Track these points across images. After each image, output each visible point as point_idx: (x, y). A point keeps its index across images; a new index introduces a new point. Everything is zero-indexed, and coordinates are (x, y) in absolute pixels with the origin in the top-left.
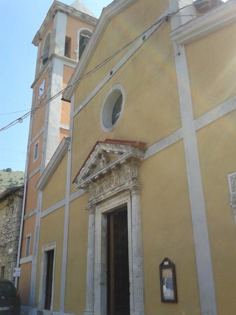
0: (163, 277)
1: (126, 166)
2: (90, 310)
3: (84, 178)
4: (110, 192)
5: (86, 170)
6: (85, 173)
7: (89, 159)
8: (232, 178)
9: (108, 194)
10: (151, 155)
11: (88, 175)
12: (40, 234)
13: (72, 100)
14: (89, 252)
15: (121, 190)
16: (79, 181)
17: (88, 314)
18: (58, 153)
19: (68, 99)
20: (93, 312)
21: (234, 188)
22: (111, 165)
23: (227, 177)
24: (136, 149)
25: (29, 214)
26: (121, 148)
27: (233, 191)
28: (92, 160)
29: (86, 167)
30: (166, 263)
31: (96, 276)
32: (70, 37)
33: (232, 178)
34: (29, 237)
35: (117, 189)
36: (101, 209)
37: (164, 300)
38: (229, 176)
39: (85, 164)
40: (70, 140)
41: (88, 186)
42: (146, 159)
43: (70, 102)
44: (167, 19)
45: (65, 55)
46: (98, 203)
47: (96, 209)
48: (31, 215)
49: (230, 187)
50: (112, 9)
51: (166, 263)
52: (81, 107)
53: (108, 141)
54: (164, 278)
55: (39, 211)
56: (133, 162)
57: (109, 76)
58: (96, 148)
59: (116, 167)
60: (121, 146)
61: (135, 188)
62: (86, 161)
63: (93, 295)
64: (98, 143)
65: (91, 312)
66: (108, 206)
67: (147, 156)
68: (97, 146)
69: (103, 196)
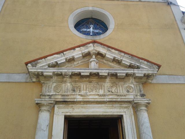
4: (97, 97)
5: (61, 59)
7: (72, 51)
9: (91, 97)
11: (56, 65)
15: (119, 100)
16: (39, 65)
29: (62, 56)
35: (111, 97)
42: (153, 84)
47: (56, 106)
61: (147, 105)
68: (91, 45)
69: (79, 97)
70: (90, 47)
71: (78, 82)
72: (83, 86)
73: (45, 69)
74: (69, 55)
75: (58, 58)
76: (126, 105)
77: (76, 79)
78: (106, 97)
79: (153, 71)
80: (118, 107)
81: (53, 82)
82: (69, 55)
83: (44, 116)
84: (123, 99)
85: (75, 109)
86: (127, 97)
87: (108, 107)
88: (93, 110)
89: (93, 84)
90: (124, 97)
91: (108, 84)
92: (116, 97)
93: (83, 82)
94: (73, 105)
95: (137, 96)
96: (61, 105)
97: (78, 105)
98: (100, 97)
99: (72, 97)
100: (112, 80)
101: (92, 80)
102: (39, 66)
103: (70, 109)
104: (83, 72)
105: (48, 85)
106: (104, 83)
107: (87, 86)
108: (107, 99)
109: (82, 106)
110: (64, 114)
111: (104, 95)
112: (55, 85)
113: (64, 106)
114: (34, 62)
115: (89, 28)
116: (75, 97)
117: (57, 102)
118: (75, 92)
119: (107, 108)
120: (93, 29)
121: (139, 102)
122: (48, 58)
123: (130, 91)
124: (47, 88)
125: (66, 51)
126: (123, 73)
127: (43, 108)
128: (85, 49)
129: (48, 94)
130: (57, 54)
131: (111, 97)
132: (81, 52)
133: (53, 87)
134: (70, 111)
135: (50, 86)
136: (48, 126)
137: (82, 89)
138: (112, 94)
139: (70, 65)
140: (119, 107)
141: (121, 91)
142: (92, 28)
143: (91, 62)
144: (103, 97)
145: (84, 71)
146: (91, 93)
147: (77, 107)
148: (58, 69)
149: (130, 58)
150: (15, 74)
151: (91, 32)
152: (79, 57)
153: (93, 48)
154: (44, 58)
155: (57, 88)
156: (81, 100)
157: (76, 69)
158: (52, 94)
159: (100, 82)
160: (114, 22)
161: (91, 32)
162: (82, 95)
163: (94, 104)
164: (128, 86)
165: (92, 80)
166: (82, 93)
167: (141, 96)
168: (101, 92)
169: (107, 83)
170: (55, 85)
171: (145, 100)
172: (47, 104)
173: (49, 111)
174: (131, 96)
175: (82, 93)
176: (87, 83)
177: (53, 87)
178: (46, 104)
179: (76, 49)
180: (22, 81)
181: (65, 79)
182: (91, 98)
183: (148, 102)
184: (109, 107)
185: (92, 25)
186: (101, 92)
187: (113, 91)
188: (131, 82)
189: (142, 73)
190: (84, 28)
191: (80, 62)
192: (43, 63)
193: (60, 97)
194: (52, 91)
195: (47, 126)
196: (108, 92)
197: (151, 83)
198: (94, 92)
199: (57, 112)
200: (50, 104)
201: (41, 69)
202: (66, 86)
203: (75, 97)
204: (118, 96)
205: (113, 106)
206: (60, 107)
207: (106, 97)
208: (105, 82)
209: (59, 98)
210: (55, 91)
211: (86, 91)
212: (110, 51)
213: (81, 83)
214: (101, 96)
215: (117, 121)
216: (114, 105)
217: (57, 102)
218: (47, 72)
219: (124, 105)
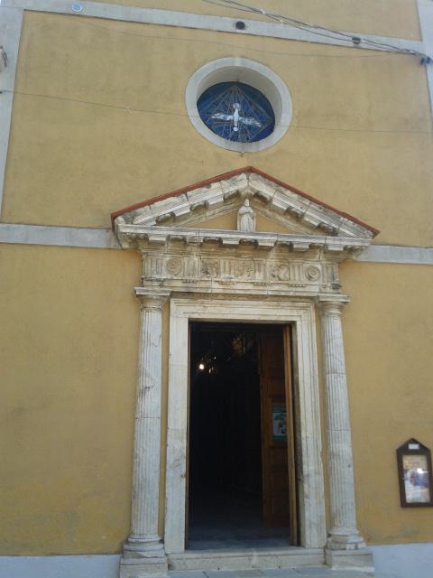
0: (404, 467)
1: (195, 250)
3: (161, 221)
4: (250, 287)
5: (180, 206)
7: (204, 189)
9: (239, 286)
11: (172, 219)
14: (151, 403)
15: (291, 294)
16: (139, 220)
20: (162, 541)
22: (297, 240)
30: (413, 447)
31: (170, 459)
35: (277, 288)
36: (192, 309)
39: (184, 191)
42: (360, 262)
46: (189, 295)
47: (173, 305)
48: (263, 148)
51: (413, 447)
54: (407, 470)
63: (162, 510)
64: (250, 170)
68: (243, 176)
75: (176, 204)
82: (198, 197)
83: (153, 319)
84: (300, 292)
86: (306, 289)
88: (241, 310)
92: (286, 288)
93: (227, 255)
95: (325, 287)
96: (182, 300)
98: (256, 288)
99: (203, 284)
102: (139, 221)
104: (227, 239)
108: (268, 291)
110: (187, 316)
112: (168, 259)
113: (187, 301)
115: (231, 112)
117: (174, 294)
122: (157, 204)
124: (154, 265)
127: (151, 305)
131: (277, 288)
135: (159, 262)
137: (222, 270)
141: (297, 278)
142: (237, 111)
144: (261, 288)
145: (228, 236)
146: (240, 279)
151: (236, 125)
161: (236, 125)
162: (222, 283)
166: (223, 277)
168: (259, 277)
171: (339, 298)
174: (314, 287)
175: (223, 277)
182: (239, 288)
186: (259, 277)
187: (282, 276)
189: (340, 246)
190: (219, 111)
193: (180, 284)
197: (355, 261)
198: (245, 278)
204: (291, 286)
205: (278, 305)
209: (179, 286)
210: (169, 272)
212: (281, 192)
214: (257, 284)
216: (282, 304)
217: (174, 294)
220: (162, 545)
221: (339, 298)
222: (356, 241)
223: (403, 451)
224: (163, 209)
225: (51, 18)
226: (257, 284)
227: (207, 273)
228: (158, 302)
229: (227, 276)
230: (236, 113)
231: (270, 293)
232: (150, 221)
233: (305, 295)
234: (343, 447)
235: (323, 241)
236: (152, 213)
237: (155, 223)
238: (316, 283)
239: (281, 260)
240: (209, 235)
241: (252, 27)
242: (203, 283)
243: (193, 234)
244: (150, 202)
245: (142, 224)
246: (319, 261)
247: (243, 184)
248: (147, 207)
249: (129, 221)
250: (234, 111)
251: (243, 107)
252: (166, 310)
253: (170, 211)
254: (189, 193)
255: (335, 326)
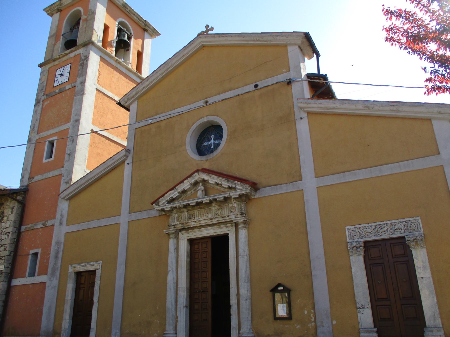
2: (172, 332)
3: (170, 202)
4: (206, 221)
5: (174, 194)
6: (172, 197)
7: (182, 184)
8: (349, 230)
9: (202, 222)
10: (263, 196)
11: (172, 200)
12: (63, 251)
13: (134, 107)
14: (171, 277)
15: (223, 221)
16: (161, 203)
17: (172, 335)
18: (110, 163)
19: (126, 105)
20: (176, 333)
21: (350, 237)
23: (345, 229)
24: (253, 188)
25: (36, 225)
26: (236, 184)
27: (349, 239)
28: (186, 185)
29: (175, 191)
30: (280, 288)
32: (109, 26)
33: (349, 230)
34: (36, 254)
35: (217, 219)
37: (276, 318)
38: (347, 228)
40: (130, 153)
41: (173, 210)
42: (256, 198)
43: (128, 110)
44: (289, 82)
45: (102, 46)
47: (180, 235)
49: (347, 236)
50: (238, 38)
51: (280, 288)
52: (150, 121)
53: (205, 171)
55: (61, 224)
56: (244, 198)
57: (202, 103)
58: (194, 175)
59: (224, 199)
60: (235, 182)
61: (245, 223)
62: (177, 185)
63: (176, 317)
64: (197, 171)
65: (173, 333)
66: (200, 233)
67: (257, 195)
68: (196, 174)
69: (193, 223)
70: (195, 176)
71: (192, 210)
72: (197, 213)
73: (165, 206)
74: (180, 188)
75: (172, 193)
76: (230, 224)
77: (190, 209)
78: (214, 220)
79: (246, 190)
80: (224, 227)
81: (175, 214)
82: (180, 188)
83: (172, 242)
84: (226, 219)
85: (194, 233)
86: (230, 217)
87: (217, 228)
88: (206, 232)
89: (204, 209)
90: (227, 218)
91: (215, 207)
92: (220, 219)
93: (196, 209)
94: (192, 231)
95: (237, 215)
96: (183, 232)
97: (195, 230)
98: (209, 221)
99: (189, 224)
100: (217, 204)
101: (201, 206)
102: (161, 204)
103: (190, 234)
104: (191, 203)
105: (172, 216)
106: (212, 208)
107: (200, 212)
108: (214, 222)
109: (198, 230)
110: (186, 238)
111: (211, 219)
112: (177, 215)
113: (185, 232)
114: (156, 202)
115: (210, 140)
116: (191, 223)
117: (181, 230)
118: (191, 219)
119: (216, 229)
120: (214, 140)
121: (237, 221)
122: (166, 195)
123: (232, 211)
124: (172, 220)
125: (177, 186)
126: (221, 197)
127: (171, 236)
128: (192, 179)
129: (172, 224)
130: (171, 190)
131: (217, 219)
132: (189, 183)
133: (176, 217)
134: (190, 236)
135: (174, 217)
136: (176, 249)
137: (196, 216)
138: (218, 216)
139: (185, 195)
140: (225, 227)
141: (225, 213)
142: (213, 138)
143: (198, 191)
144: (211, 221)
145: (191, 202)
146: (203, 218)
147: (194, 231)
148: (174, 204)
149: (227, 180)
150: (151, 210)
151: (212, 145)
152: (189, 188)
153: (198, 177)
154: (163, 196)
155: (178, 218)
156: (195, 225)
157: (185, 202)
158: (175, 224)
159: (209, 207)
160: (227, 131)
161: (212, 145)
162: (195, 222)
163: (207, 227)
164: (231, 206)
165: (201, 206)
166: (196, 220)
167: (241, 215)
168: (210, 216)
169: (215, 207)
170: (177, 215)
171: (241, 219)
172: (172, 233)
173: (175, 238)
174: (233, 216)
175: (196, 220)
176: (199, 210)
177: (176, 217)
178: (171, 233)
179: (184, 181)
180: (157, 215)
181: (182, 210)
182: (203, 223)
183: (244, 220)
184: (218, 228)
185: (213, 134)
186: (210, 216)
187: (219, 213)
188: (233, 202)
189: (236, 195)
190: (206, 141)
191: (192, 190)
192: (163, 201)
193: (181, 225)
194: (176, 221)
195: (175, 249)
196: (215, 215)
197: (254, 199)
198: (205, 217)
199: (181, 237)
200: (175, 233)
201: (163, 206)
202: (185, 215)
203: (191, 223)
204: (223, 217)
205: (220, 227)
206: (183, 233)
207: (213, 221)
208: (212, 206)
209: (180, 226)
210: (177, 221)
211: (199, 217)
212: (211, 177)
213: (195, 211)
214: (209, 220)
215: (225, 237)
216: (221, 226)
217: (181, 230)
218: (167, 208)
219: (229, 225)
220: (175, 335)
221: (241, 219)
222: (243, 191)
223: (274, 290)
224: (168, 196)
225: (143, 128)
226: (209, 220)
227: (191, 219)
228: (174, 235)
229: (198, 218)
230: (212, 140)
231: (215, 223)
232: (165, 202)
233: (229, 220)
234: (244, 291)
235: (228, 195)
236: (165, 199)
237: (167, 203)
238: (234, 213)
239: (219, 206)
240: (184, 203)
241: (210, 100)
242: (189, 223)
243: (178, 204)
244: (163, 195)
245: (162, 204)
246: (234, 203)
247: (197, 177)
248: (162, 197)
249: (158, 204)
250: (212, 139)
251: (215, 136)
252: (177, 237)
253: (171, 197)
254: (176, 188)
255: (243, 232)
